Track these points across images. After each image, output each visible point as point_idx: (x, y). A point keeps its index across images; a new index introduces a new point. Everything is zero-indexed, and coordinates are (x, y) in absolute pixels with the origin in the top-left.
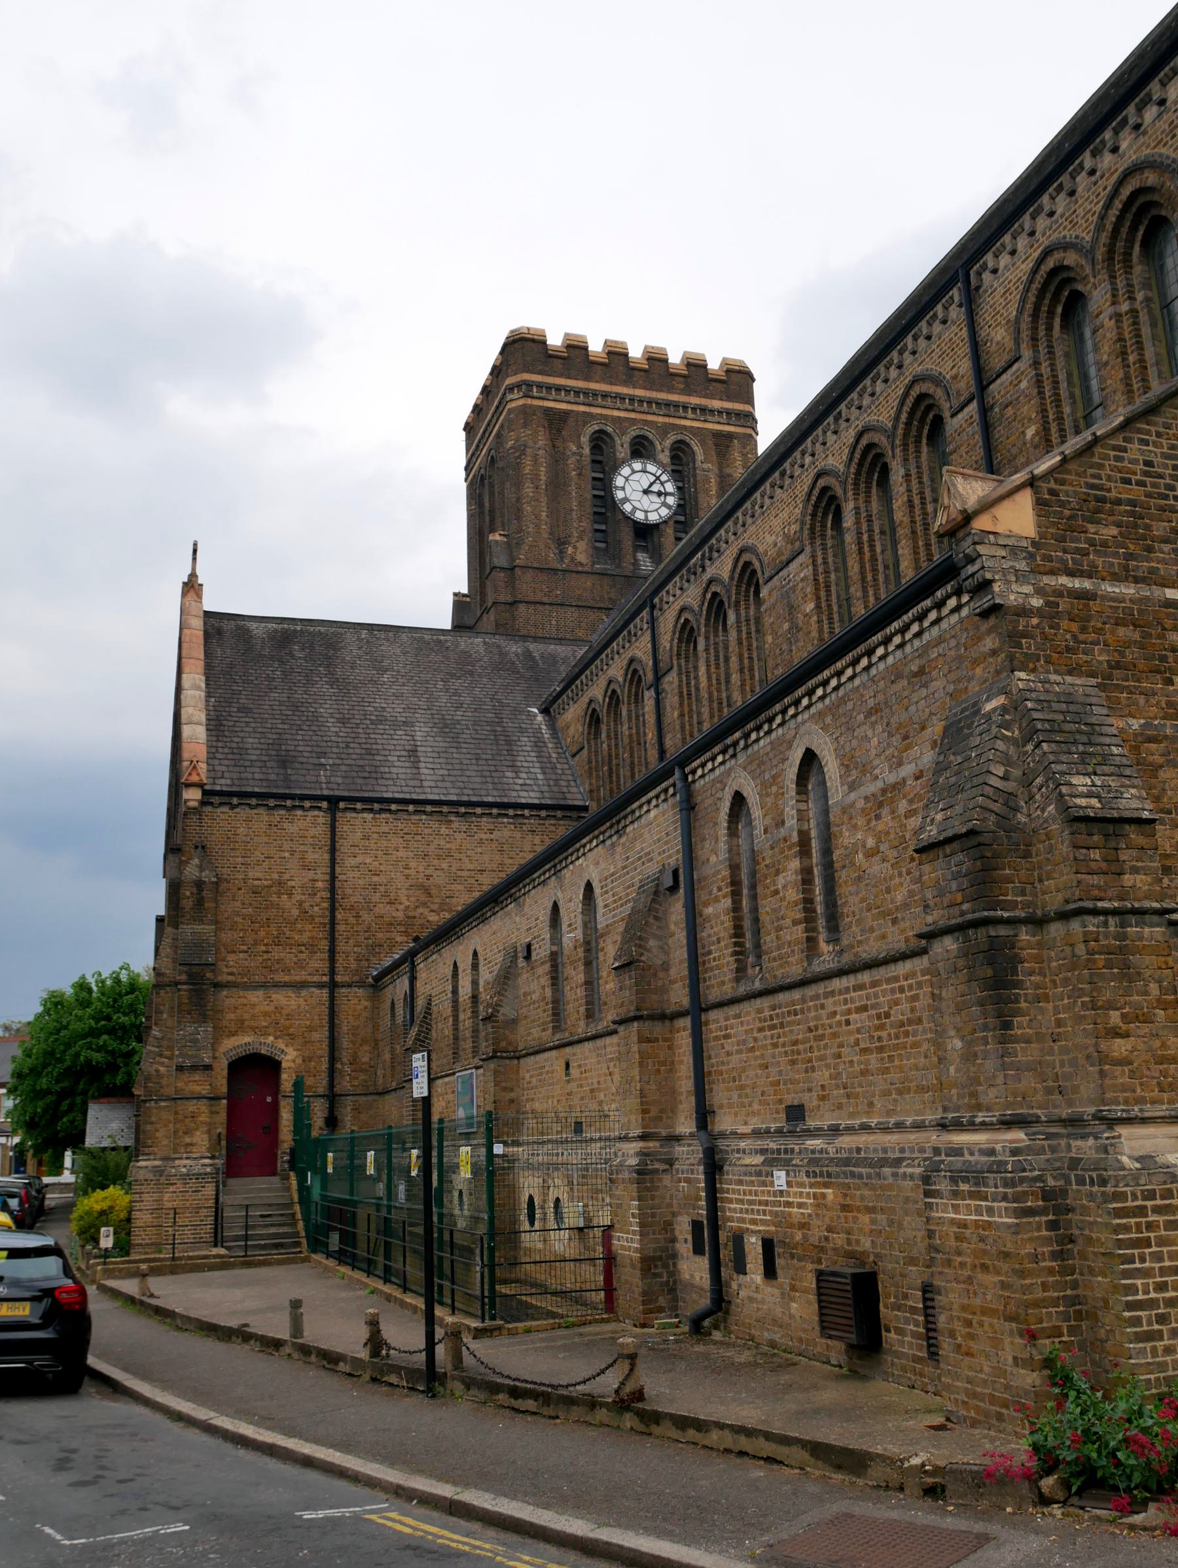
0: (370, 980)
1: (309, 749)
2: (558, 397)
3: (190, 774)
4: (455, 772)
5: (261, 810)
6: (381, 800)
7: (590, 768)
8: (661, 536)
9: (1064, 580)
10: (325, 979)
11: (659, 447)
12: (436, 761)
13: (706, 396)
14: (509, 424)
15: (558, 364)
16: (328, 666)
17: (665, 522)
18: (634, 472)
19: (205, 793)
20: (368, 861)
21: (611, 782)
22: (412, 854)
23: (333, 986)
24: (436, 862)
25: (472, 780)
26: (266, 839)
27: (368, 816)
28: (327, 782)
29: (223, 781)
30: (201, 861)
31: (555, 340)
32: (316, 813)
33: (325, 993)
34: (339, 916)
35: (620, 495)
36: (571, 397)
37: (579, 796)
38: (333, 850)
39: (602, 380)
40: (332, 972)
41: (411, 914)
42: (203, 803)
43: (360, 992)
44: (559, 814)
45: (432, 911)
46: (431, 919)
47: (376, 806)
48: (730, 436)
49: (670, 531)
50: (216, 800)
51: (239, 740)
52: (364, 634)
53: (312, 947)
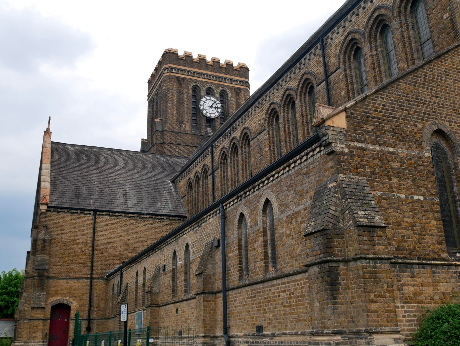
0: (106, 277)
1: (87, 192)
5: (69, 214)
7: (188, 203)
9: (356, 143)
10: (89, 276)
13: (232, 75)
14: (164, 81)
18: (207, 100)
19: (48, 207)
20: (107, 233)
21: (195, 208)
22: (123, 232)
23: (92, 279)
24: (131, 234)
26: (69, 224)
27: (108, 217)
28: (93, 205)
30: (45, 232)
31: (181, 53)
32: (89, 215)
33: (89, 281)
34: (95, 253)
35: (202, 107)
38: (94, 229)
39: (197, 68)
40: (92, 274)
41: (122, 253)
42: (47, 211)
43: (102, 281)
44: (176, 218)
46: (129, 255)
47: (111, 214)
48: (240, 89)
49: (219, 121)
50: (52, 210)
52: (109, 152)
53: (84, 264)
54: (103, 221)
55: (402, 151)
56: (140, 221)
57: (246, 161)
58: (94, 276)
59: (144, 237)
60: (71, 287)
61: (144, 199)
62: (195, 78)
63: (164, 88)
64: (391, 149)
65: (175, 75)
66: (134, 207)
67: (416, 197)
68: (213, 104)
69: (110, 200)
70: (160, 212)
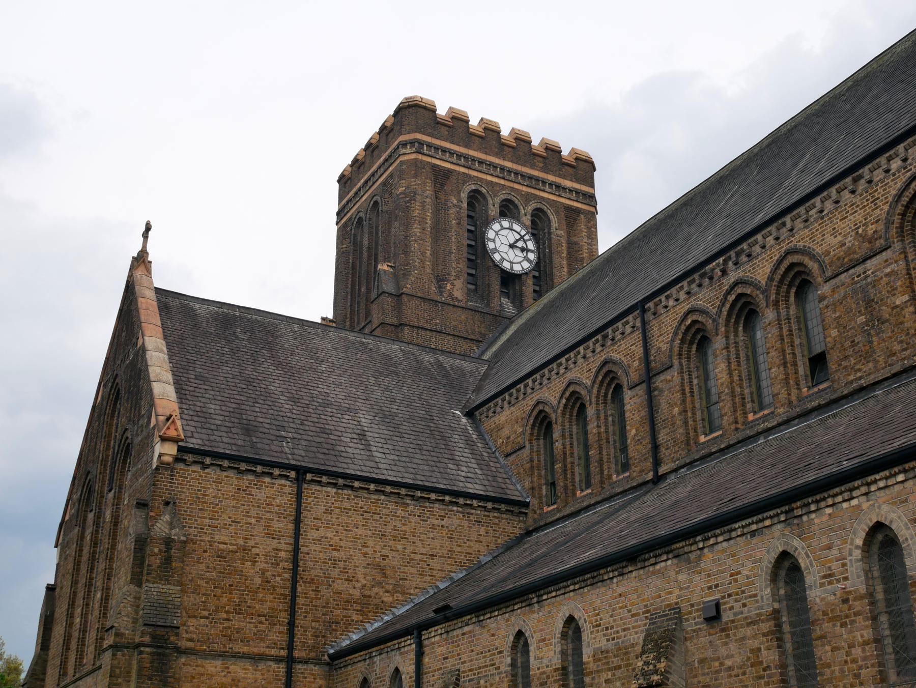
0: (326, 657)
1: (268, 421)
2: (444, 157)
3: (168, 428)
4: (404, 459)
5: (231, 473)
6: (345, 476)
7: (532, 467)
8: (522, 285)
10: (283, 653)
11: (522, 211)
12: (385, 446)
13: (559, 176)
14: (400, 173)
15: (444, 130)
16: (270, 349)
17: (526, 273)
18: (502, 228)
19: (180, 449)
20: (329, 535)
21: (566, 479)
22: (370, 533)
23: (290, 661)
24: (391, 543)
25: (421, 467)
26: (233, 503)
27: (332, 491)
28: (292, 452)
29: (194, 441)
30: (172, 518)
31: (442, 111)
32: (283, 482)
33: (282, 668)
34: (299, 589)
35: (491, 245)
36: (454, 159)
37: (517, 493)
38: (297, 521)
39: (479, 149)
40: (291, 647)
41: (367, 593)
42: (177, 460)
43: (316, 669)
44: (503, 507)
45: (387, 592)
46: (385, 599)
47: (341, 481)
48: (578, 211)
49: (530, 282)
50: (190, 458)
51: (201, 404)
52: (296, 327)
53: (271, 619)
54: (320, 498)
56: (412, 506)
57: (792, 342)
58: (296, 654)
59: (424, 551)
61: (410, 450)
62: (475, 174)
63: (401, 190)
65: (429, 159)
66: (394, 468)
68: (517, 241)
69: (329, 447)
70: (460, 486)
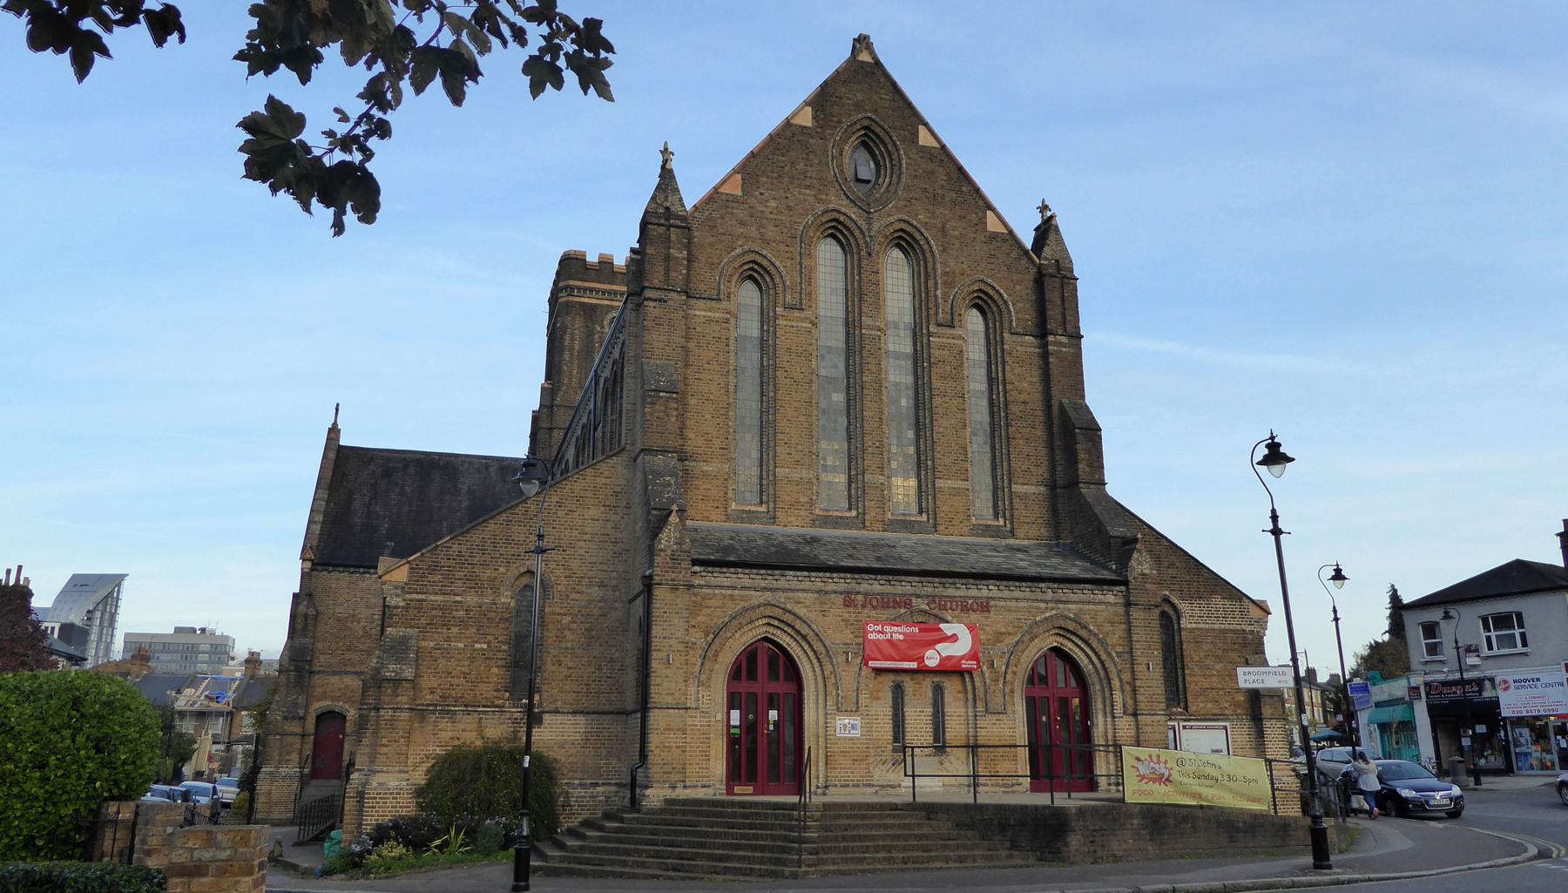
55: (471, 599)
60: (347, 687)
64: (458, 598)
67: (477, 646)
